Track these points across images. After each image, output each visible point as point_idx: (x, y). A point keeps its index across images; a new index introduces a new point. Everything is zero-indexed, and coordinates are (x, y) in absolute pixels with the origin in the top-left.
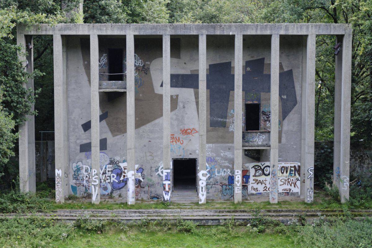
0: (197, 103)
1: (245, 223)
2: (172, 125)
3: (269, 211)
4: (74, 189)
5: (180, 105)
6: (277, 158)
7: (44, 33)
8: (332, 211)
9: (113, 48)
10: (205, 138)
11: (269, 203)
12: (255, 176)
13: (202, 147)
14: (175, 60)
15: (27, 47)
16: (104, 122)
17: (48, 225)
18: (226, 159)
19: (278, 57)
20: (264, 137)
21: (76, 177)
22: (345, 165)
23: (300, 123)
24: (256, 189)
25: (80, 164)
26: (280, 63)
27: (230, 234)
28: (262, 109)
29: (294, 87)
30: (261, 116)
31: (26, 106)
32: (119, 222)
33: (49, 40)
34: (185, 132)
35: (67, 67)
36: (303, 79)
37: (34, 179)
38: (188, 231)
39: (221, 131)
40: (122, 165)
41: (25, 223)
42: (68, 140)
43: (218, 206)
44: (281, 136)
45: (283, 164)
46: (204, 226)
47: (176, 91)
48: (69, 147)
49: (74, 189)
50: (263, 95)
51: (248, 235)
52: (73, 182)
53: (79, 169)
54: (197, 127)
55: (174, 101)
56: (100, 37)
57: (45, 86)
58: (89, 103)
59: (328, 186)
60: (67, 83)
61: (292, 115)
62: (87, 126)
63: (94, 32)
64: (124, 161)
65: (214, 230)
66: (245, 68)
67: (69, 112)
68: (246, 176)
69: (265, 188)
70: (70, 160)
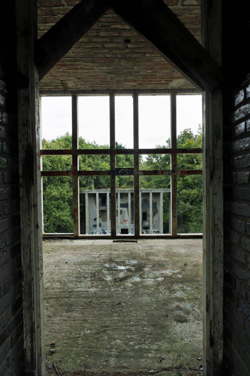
0: (128, 212)
5: (123, 213)
7: (82, 193)
9: (103, 197)
13: (130, 226)
14: (122, 199)
16: (100, 218)
19: (152, 198)
20: (148, 223)
23: (159, 218)
26: (153, 200)
28: (148, 214)
29: (157, 207)
30: (185, 154)
33: (84, 194)
34: (125, 221)
36: (159, 205)
40: (106, 231)
42: (90, 224)
44: (195, 149)
45: (154, 230)
47: (122, 209)
48: (90, 225)
54: (128, 219)
55: (121, 212)
56: (99, 194)
58: (96, 213)
60: (89, 207)
61: (156, 216)
62: (95, 219)
63: (97, 192)
64: (106, 230)
66: (142, 201)
67: (90, 215)
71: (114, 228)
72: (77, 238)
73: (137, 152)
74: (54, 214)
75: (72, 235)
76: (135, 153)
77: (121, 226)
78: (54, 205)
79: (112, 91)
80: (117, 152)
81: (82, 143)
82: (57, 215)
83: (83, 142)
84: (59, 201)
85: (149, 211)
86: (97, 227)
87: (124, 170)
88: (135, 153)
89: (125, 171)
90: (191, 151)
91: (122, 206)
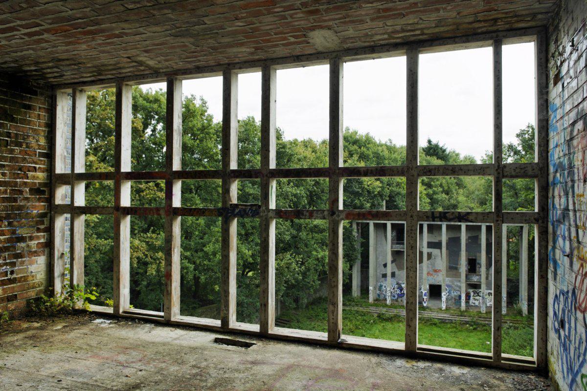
1: (467, 323)
2: (428, 267)
3: (480, 317)
4: (379, 295)
5: (433, 257)
6: (485, 288)
8: (517, 321)
10: (445, 275)
11: (480, 312)
12: (473, 296)
13: (444, 280)
14: (430, 235)
15: (357, 227)
16: (394, 264)
17: (364, 315)
18: (457, 286)
19: (485, 235)
20: (478, 277)
21: (380, 290)
22: (525, 296)
24: (474, 303)
25: (382, 283)
27: (457, 329)
28: (477, 261)
31: (356, 256)
32: (399, 316)
34: (436, 271)
35: (377, 236)
37: (359, 289)
38: (435, 324)
39: (454, 272)
41: (354, 312)
43: (452, 312)
46: (443, 322)
47: (430, 250)
49: (379, 295)
50: (478, 254)
51: (468, 330)
52: (378, 292)
53: (381, 286)
54: (441, 268)
55: (430, 256)
57: (365, 246)
59: (515, 306)
62: (385, 265)
65: (449, 326)
67: (377, 258)
68: (468, 296)
69: (479, 303)
70: (377, 281)
71: (225, 314)
72: (167, 323)
73: (267, 175)
74: (314, 253)
75: (162, 317)
76: (263, 177)
77: (428, 280)
78: (317, 240)
79: (225, 66)
80: (232, 175)
81: (369, 144)
82: (319, 256)
83: (370, 141)
84: (324, 234)
85: (480, 257)
86: (388, 278)
87: (244, 207)
88: (263, 177)
89: (245, 210)
90: (367, 172)
91: (431, 245)
